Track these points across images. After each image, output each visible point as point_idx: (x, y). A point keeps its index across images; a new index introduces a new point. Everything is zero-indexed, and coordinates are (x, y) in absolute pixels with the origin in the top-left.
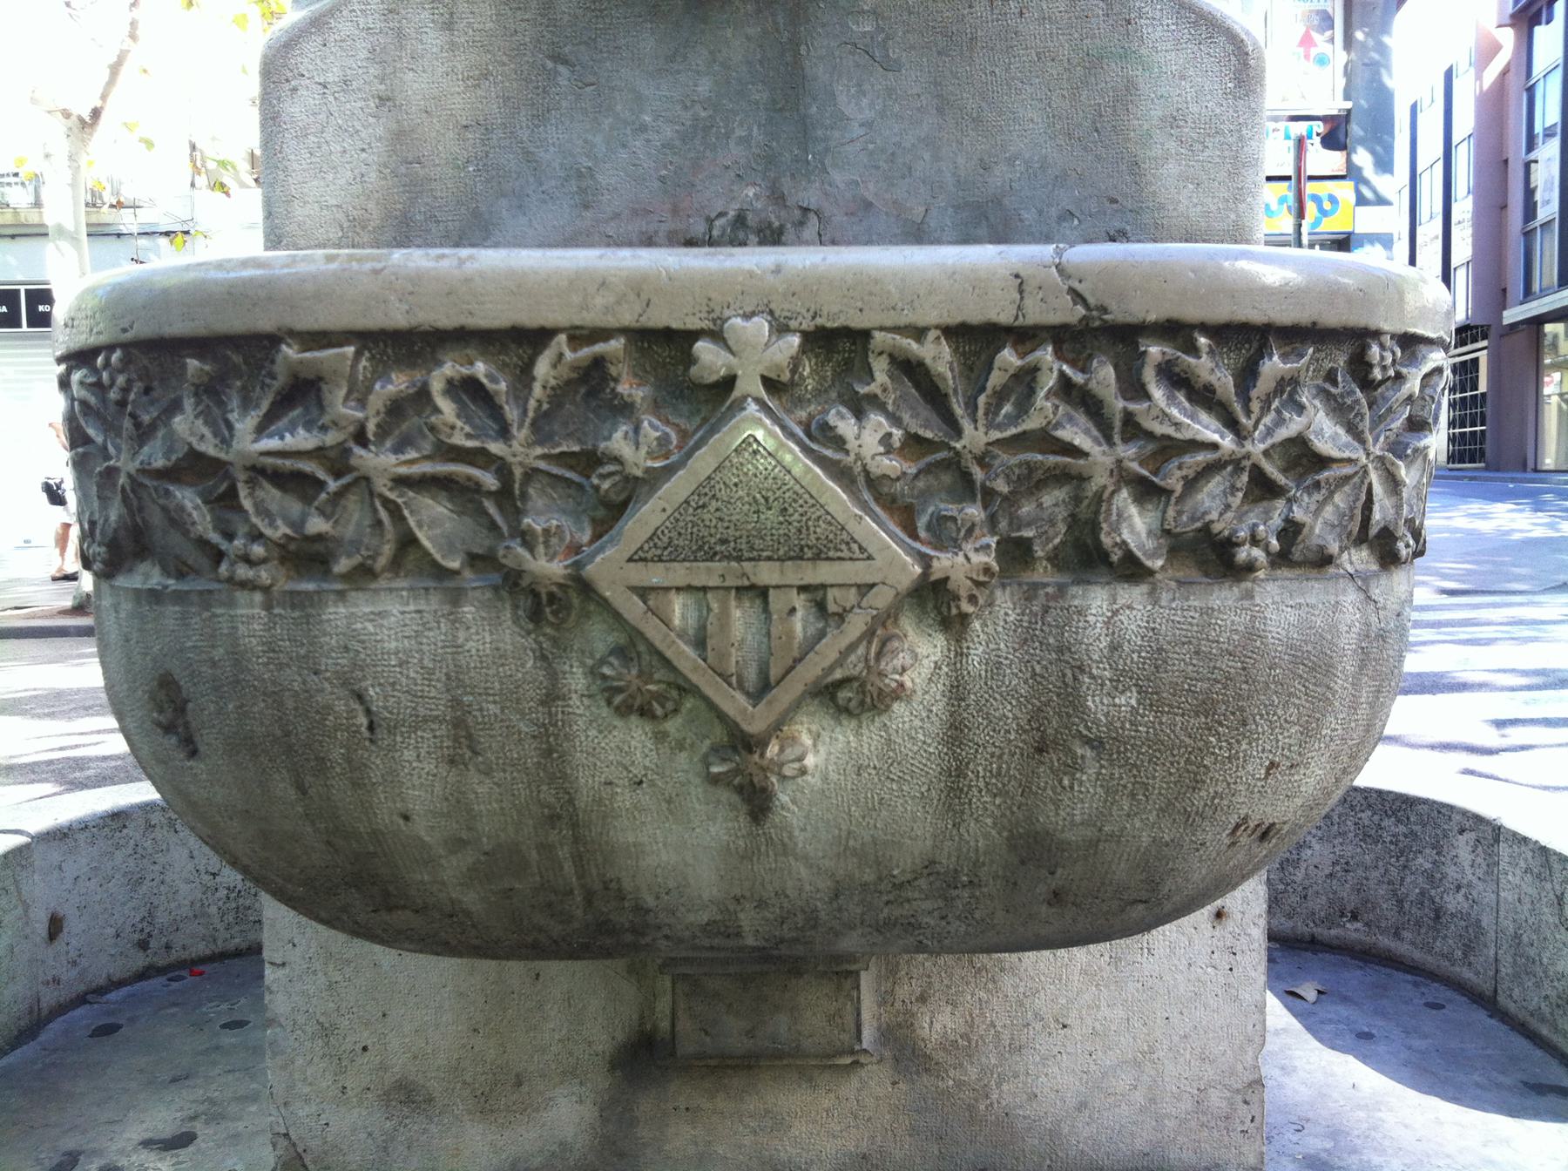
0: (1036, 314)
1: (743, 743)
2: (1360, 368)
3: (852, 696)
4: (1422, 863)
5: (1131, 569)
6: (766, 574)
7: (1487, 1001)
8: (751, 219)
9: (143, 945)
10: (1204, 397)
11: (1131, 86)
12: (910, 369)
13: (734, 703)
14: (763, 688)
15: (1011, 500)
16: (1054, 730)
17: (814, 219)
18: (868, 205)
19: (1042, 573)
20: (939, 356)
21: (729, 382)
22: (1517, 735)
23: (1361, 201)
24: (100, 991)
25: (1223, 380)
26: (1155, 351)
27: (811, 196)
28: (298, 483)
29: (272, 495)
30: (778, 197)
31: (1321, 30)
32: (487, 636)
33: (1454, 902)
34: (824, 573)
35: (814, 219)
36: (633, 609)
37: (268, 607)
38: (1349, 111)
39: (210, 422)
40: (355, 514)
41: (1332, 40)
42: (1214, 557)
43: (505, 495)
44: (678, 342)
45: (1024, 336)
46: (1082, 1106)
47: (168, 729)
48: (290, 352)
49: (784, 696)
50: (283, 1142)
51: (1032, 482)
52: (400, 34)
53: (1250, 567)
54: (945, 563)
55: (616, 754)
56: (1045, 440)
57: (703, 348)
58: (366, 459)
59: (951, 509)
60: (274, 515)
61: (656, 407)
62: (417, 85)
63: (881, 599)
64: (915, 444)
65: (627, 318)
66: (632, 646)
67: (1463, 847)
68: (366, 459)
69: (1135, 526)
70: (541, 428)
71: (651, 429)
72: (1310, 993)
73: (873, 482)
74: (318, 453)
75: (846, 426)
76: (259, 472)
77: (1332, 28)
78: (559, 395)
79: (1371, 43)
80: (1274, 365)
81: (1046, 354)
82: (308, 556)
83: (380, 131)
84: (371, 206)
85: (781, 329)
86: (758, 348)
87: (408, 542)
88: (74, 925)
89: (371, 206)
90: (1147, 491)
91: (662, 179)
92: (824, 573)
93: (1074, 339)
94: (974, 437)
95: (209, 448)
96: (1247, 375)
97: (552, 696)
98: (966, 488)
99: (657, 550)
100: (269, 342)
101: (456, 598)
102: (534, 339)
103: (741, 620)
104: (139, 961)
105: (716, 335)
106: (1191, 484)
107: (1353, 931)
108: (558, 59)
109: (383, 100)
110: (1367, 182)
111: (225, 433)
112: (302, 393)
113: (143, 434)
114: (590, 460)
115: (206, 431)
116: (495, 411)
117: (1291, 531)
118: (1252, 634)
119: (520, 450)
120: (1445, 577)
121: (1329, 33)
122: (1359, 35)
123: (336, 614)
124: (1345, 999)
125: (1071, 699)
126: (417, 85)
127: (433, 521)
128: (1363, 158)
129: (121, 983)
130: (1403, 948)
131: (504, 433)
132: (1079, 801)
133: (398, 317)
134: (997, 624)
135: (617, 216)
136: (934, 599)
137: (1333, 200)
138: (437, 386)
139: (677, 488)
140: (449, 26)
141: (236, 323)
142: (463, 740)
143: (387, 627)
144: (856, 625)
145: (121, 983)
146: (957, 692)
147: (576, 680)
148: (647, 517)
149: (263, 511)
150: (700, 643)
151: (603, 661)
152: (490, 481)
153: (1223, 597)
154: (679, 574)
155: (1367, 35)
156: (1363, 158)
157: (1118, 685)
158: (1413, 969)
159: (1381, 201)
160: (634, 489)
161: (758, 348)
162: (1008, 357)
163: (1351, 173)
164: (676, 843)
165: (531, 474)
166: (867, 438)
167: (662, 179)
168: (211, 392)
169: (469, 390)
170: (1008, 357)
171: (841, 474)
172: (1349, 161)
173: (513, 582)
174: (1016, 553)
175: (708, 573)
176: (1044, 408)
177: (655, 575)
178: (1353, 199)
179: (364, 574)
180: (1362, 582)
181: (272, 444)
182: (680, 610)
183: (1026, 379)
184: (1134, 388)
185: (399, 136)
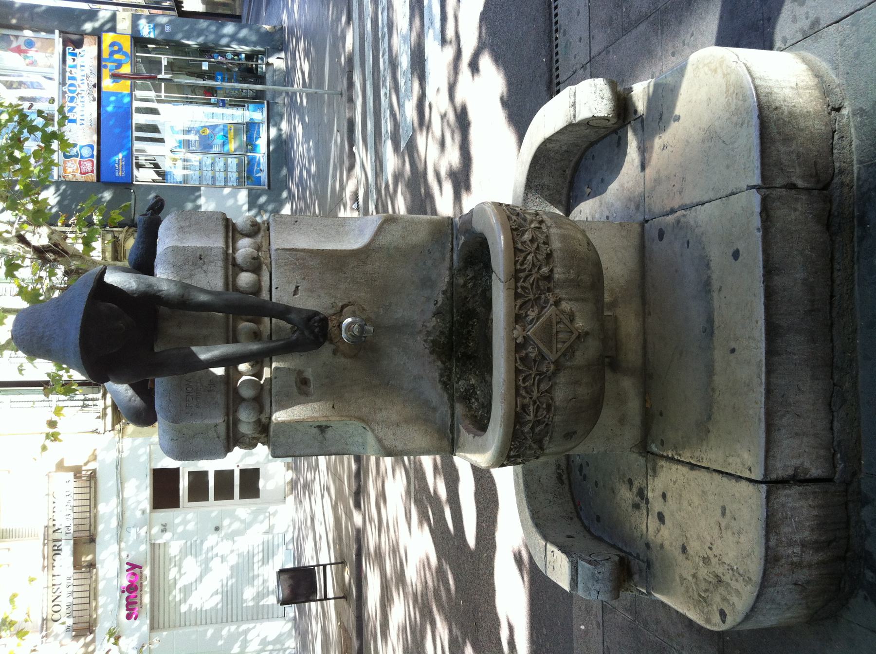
0: (513, 286)
1: (579, 337)
2: (516, 229)
3: (572, 318)
4: (552, 154)
5: (552, 271)
6: (554, 331)
7: (592, 144)
9: (571, 519)
10: (525, 258)
11: (395, 247)
12: (521, 308)
13: (574, 337)
14: (571, 332)
15: (541, 290)
16: (574, 283)
19: (552, 285)
20: (519, 302)
21: (524, 337)
22: (450, 33)
23: (113, 29)
24: (585, 527)
25: (523, 255)
26: (518, 267)
27: (420, 324)
28: (538, 408)
29: (539, 414)
30: (421, 331)
31: (11, 42)
32: (562, 378)
33: (564, 148)
34: (554, 322)
36: (559, 353)
38: (61, 32)
40: (543, 400)
41: (17, 37)
42: (549, 256)
43: (540, 375)
45: (516, 288)
46: (625, 264)
47: (571, 437)
48: (518, 409)
49: (573, 329)
51: (538, 287)
52: (383, 421)
53: (551, 250)
54: (551, 302)
55: (581, 357)
57: (518, 341)
58: (534, 398)
59: (542, 301)
60: (543, 412)
61: (526, 349)
62: (395, 417)
63: (558, 312)
64: (532, 307)
65: (513, 354)
66: (564, 355)
67: (549, 146)
68: (534, 398)
69: (545, 270)
70: (531, 369)
71: (530, 349)
72: (589, 190)
73: (540, 313)
74: (534, 405)
75: (531, 318)
76: (536, 416)
78: (525, 366)
79: (18, 15)
80: (519, 246)
81: (519, 284)
82: (549, 408)
85: (515, 329)
86: (518, 332)
87: (546, 391)
88: (569, 533)
90: (540, 268)
92: (554, 322)
93: (517, 279)
94: (531, 296)
95: (530, 425)
96: (521, 251)
97: (571, 368)
98: (539, 298)
99: (550, 349)
100: (516, 413)
101: (556, 383)
103: (561, 336)
104: (576, 519)
105: (516, 339)
106: (539, 261)
107: (568, 172)
108: (388, 384)
109: (398, 426)
110: (103, 25)
111: (529, 421)
112: (524, 407)
113: (526, 439)
114: (535, 361)
116: (527, 376)
117: (545, 243)
118: (560, 250)
119: (533, 372)
120: (339, 19)
121: (12, 38)
122: (14, 21)
123: (557, 404)
124: (590, 180)
125: (572, 280)
126: (395, 417)
127: (544, 386)
128: (88, 27)
129: (583, 523)
130: (575, 160)
131: (531, 375)
132: (586, 278)
133: (514, 391)
134: (561, 293)
136: (557, 303)
137: (113, 44)
138: (523, 385)
139: (541, 346)
140: (381, 410)
141: (513, 417)
142: (577, 383)
143: (560, 395)
144: (562, 316)
145: (583, 523)
146: (570, 300)
147: (569, 364)
148: (545, 350)
150: (564, 342)
152: (538, 377)
153: (555, 255)
154: (554, 345)
155: (13, 17)
156: (88, 27)
157: (569, 273)
158: (581, 158)
159: (113, 18)
160: (540, 353)
161: (518, 332)
162: (519, 290)
163: (97, 34)
164: (589, 351)
165: (537, 370)
166: (532, 314)
168: (522, 424)
169: (524, 380)
170: (519, 290)
171: (538, 319)
172: (90, 34)
173: (554, 374)
174: (549, 290)
175: (554, 341)
176: (527, 285)
177: (554, 350)
178: (112, 34)
179: (552, 398)
180: (548, 228)
182: (559, 346)
183: (523, 288)
184: (524, 270)
185: (406, 421)
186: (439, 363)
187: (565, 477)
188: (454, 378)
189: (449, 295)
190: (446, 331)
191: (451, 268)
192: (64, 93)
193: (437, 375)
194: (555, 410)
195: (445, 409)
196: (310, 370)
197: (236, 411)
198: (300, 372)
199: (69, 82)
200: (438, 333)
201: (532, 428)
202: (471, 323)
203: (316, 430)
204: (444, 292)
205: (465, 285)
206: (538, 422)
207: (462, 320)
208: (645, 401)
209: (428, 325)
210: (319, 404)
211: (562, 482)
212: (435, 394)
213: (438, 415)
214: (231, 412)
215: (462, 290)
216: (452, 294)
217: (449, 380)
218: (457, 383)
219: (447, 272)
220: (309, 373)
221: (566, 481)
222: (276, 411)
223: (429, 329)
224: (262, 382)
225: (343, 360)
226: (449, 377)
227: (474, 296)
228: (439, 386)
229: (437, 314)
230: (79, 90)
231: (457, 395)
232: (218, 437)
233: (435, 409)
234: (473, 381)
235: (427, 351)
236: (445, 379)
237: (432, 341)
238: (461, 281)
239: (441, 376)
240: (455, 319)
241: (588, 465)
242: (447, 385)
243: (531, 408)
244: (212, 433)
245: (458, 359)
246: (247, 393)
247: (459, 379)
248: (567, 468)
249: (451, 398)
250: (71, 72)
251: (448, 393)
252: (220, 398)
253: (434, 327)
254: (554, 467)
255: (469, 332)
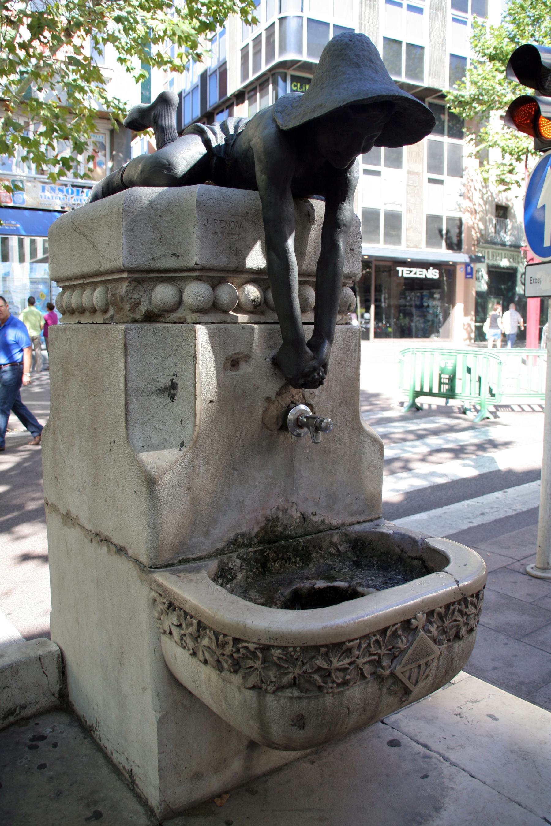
8: (281, 508)
11: (361, 459)
17: (295, 505)
18: (307, 499)
27: (294, 499)
30: (287, 500)
35: (295, 505)
37: (333, 696)
39: (325, 661)
41: (105, 156)
44: (408, 622)
45: (453, 603)
48: (347, 644)
50: (163, 803)
52: (194, 468)
56: (455, 620)
57: (413, 621)
60: (338, 677)
77: (105, 150)
83: (188, 498)
84: (185, 521)
89: (185, 521)
91: (260, 500)
95: (326, 666)
102: (386, 629)
105: (415, 618)
108: (235, 469)
113: (303, 664)
115: (325, 663)
135: (249, 513)
140: (207, 464)
147: (385, 691)
149: (337, 677)
150: (409, 678)
151: (391, 686)
160: (403, 652)
167: (260, 500)
181: (341, 663)
185: (193, 498)
186: (256, 530)
187: (11, 719)
188: (241, 552)
189: (321, 528)
190: (288, 532)
191: (344, 525)
192: (66, 185)
193: (244, 529)
194: (339, 693)
195: (207, 547)
196: (250, 370)
197: (199, 279)
198: (247, 358)
199: (75, 189)
200: (285, 522)
201: (319, 669)
202: (298, 559)
203: (165, 381)
204: (323, 522)
205: (332, 544)
206: (327, 674)
207: (300, 548)
208: (219, 796)
209: (294, 509)
210: (215, 382)
211: (5, 718)
212: (223, 531)
213: (200, 539)
214: (203, 274)
215: (328, 541)
216: (321, 532)
217: (239, 546)
218: (237, 557)
219: (340, 522)
220: (245, 369)
221: (6, 722)
222: (208, 329)
223: (289, 511)
224: (231, 312)
225: (260, 410)
226: (243, 545)
227: (323, 557)
228: (232, 535)
229: (304, 517)
230: (69, 196)
231: (225, 560)
232: (153, 259)
233: (207, 534)
234: (239, 576)
235: (268, 512)
236: (240, 540)
237: (277, 518)
238: (335, 539)
239: (243, 535)
240: (299, 539)
241: (55, 745)
242: (234, 543)
243: (347, 661)
244: (160, 250)
245: (262, 552)
246: (225, 293)
247: (242, 558)
248: (22, 719)
249: (219, 553)
250: (83, 192)
251: (224, 548)
252: (222, 261)
253: (291, 516)
254: (22, 702)
255: (289, 558)
